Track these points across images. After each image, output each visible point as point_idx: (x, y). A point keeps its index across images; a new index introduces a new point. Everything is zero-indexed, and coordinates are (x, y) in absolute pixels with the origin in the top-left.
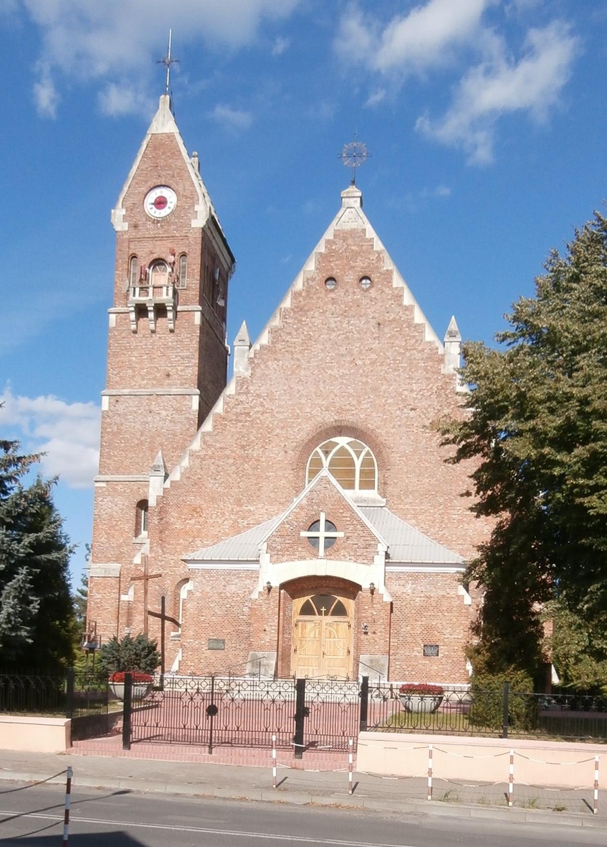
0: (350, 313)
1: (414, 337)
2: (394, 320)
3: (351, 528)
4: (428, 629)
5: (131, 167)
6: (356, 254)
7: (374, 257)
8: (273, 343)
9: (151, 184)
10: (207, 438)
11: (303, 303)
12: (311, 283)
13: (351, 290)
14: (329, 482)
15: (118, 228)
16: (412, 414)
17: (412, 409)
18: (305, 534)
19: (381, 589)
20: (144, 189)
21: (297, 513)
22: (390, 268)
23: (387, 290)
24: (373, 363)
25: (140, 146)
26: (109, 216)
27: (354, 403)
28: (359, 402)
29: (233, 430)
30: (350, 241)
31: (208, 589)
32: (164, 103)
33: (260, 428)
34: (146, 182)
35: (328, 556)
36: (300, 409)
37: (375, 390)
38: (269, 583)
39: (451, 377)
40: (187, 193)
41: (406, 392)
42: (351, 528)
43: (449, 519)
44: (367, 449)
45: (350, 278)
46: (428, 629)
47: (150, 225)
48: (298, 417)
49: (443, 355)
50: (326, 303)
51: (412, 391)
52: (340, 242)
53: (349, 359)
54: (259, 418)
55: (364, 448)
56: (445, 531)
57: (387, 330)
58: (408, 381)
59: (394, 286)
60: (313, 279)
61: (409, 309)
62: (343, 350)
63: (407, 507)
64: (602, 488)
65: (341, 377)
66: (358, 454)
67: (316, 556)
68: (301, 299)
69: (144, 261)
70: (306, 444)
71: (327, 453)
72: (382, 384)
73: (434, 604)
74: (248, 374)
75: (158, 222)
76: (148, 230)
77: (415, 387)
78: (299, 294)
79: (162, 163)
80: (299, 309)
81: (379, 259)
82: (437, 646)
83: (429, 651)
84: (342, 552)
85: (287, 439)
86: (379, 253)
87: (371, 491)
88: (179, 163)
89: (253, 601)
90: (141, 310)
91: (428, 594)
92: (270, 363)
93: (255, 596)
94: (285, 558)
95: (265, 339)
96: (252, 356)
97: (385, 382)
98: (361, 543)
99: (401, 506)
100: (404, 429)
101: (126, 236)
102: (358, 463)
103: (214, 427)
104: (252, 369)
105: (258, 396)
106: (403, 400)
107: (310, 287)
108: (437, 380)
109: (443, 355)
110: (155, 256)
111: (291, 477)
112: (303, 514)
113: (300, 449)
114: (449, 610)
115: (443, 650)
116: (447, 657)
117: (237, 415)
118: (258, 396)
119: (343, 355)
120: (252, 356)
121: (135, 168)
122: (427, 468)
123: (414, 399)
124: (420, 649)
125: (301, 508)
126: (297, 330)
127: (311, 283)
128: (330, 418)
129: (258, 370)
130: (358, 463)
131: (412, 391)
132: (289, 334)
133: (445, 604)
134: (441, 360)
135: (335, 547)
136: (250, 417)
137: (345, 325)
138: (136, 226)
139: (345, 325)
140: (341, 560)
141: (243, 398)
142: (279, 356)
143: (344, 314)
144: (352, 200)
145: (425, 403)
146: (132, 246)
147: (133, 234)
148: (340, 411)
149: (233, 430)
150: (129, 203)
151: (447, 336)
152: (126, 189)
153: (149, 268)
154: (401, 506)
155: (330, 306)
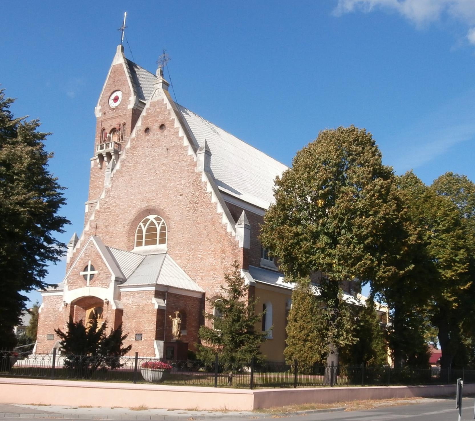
0: (156, 145)
1: (183, 154)
2: (174, 146)
3: (101, 268)
4: (139, 324)
5: (104, 84)
6: (159, 113)
7: (166, 113)
8: (121, 167)
9: (112, 91)
10: (92, 224)
11: (135, 144)
12: (139, 133)
13: (156, 133)
14: (93, 244)
15: (97, 116)
16: (181, 197)
17: (181, 195)
18: (83, 273)
19: (112, 302)
20: (109, 94)
21: (80, 262)
22: (174, 118)
23: (172, 130)
24: (164, 172)
25: (108, 72)
26: (94, 110)
27: (155, 195)
28: (157, 194)
30: (157, 107)
31: (49, 307)
34: (110, 90)
36: (131, 202)
37: (164, 186)
38: (38, 303)
39: (200, 174)
40: (127, 92)
41: (178, 186)
42: (101, 268)
43: (196, 258)
44: (163, 220)
45: (156, 126)
46: (139, 324)
48: (130, 207)
49: (196, 162)
50: (145, 142)
51: (181, 184)
52: (152, 108)
53: (153, 171)
54: (113, 210)
55: (161, 220)
56: (194, 265)
58: (180, 179)
60: (140, 130)
61: (181, 138)
63: (177, 252)
64: (346, 227)
65: (150, 181)
66: (159, 223)
67: (86, 285)
68: (134, 142)
69: (108, 131)
70: (133, 221)
71: (145, 225)
72: (168, 183)
73: (141, 309)
74: (110, 186)
75: (114, 109)
76: (109, 114)
77: (183, 182)
78: (133, 139)
79: (117, 79)
80: (133, 148)
81: (169, 114)
82: (141, 334)
83: (138, 337)
84: (97, 282)
85: (125, 219)
86: (169, 110)
87: (155, 246)
88: (124, 77)
90: (101, 157)
92: (119, 179)
93: (61, 309)
94: (74, 287)
95: (118, 167)
97: (169, 181)
100: (177, 207)
101: (100, 120)
102: (159, 229)
103: (95, 217)
105: (114, 197)
107: (138, 135)
108: (193, 176)
109: (196, 162)
110: (112, 127)
111: (126, 241)
112: (82, 262)
113: (130, 224)
115: (144, 336)
116: (146, 340)
117: (105, 209)
118: (114, 197)
119: (151, 169)
120: (112, 176)
121: (105, 84)
122: (187, 228)
124: (134, 336)
125: (82, 259)
126: (131, 159)
127: (139, 133)
128: (143, 205)
129: (114, 184)
130: (159, 229)
131: (181, 184)
132: (128, 162)
133: (146, 308)
134: (195, 165)
135: (94, 279)
137: (152, 153)
138: (105, 114)
139: (152, 153)
140: (96, 286)
141: (107, 200)
143: (152, 147)
144: (158, 85)
145: (187, 191)
146: (103, 124)
147: (104, 117)
149: (103, 218)
150: (102, 103)
151: (198, 150)
152: (101, 95)
153: (110, 133)
155: (146, 143)
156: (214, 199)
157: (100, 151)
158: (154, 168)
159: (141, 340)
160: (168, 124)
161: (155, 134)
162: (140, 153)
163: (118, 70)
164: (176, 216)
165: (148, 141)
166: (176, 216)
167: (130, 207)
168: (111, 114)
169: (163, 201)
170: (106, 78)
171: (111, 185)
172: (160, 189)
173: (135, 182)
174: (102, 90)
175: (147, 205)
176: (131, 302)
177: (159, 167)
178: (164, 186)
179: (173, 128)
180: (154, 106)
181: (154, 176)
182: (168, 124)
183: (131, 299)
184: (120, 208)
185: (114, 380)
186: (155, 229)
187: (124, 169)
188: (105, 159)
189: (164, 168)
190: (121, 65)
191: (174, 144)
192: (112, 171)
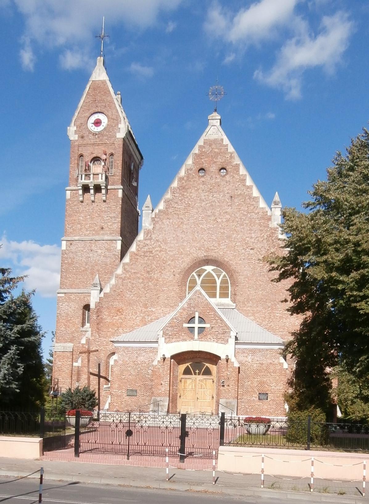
0: (214, 190)
1: (253, 205)
2: (241, 194)
4: (261, 383)
6: (218, 154)
7: (228, 156)
9: (92, 111)
11: (185, 184)
12: (190, 172)
13: (214, 176)
14: (201, 293)
15: (72, 138)
16: (252, 252)
18: (186, 325)
19: (232, 359)
20: (87, 114)
22: (238, 163)
23: (236, 176)
24: (228, 221)
25: (85, 88)
26: (66, 131)
27: (216, 245)
28: (219, 245)
29: (142, 262)
30: (213, 146)
32: (100, 61)
33: (158, 261)
34: (89, 110)
35: (200, 339)
36: (183, 249)
39: (275, 229)
40: (114, 117)
42: (214, 321)
43: (274, 316)
44: (224, 273)
45: (214, 169)
46: (261, 383)
47: (91, 136)
48: (182, 253)
49: (271, 216)
50: (199, 184)
51: (251, 238)
52: (207, 147)
53: (213, 218)
54: (158, 254)
55: (222, 273)
57: (236, 200)
58: (249, 232)
59: (241, 173)
60: (191, 169)
61: (250, 188)
62: (209, 213)
66: (219, 276)
67: (193, 339)
68: (184, 181)
70: (187, 270)
71: (199, 276)
72: (233, 234)
74: (151, 227)
75: (96, 134)
76: (90, 139)
77: (253, 235)
78: (182, 178)
79: (98, 98)
80: (182, 188)
81: (231, 157)
82: (267, 394)
83: (262, 397)
84: (209, 336)
86: (231, 153)
88: (109, 99)
89: (154, 367)
90: (86, 189)
91: (261, 362)
92: (164, 221)
93: (155, 363)
94: (174, 340)
95: (161, 206)
96: (154, 216)
98: (221, 331)
99: (245, 308)
100: (246, 261)
101: (76, 143)
102: (218, 282)
103: (131, 260)
104: (154, 224)
106: (246, 244)
107: (189, 174)
108: (267, 231)
109: (271, 216)
110: (94, 155)
111: (177, 291)
112: (185, 313)
113: (183, 273)
114: (274, 372)
115: (270, 396)
116: (273, 400)
117: (144, 252)
119: (209, 216)
120: (154, 216)
121: (82, 101)
122: (260, 285)
123: (253, 243)
124: (256, 395)
127: (190, 172)
128: (202, 254)
129: (157, 225)
130: (218, 282)
131: (251, 238)
132: (177, 203)
133: (272, 368)
134: (269, 219)
136: (152, 253)
137: (210, 198)
138: (82, 137)
139: (210, 198)
140: (208, 341)
141: (148, 242)
142: (170, 216)
143: (210, 191)
145: (259, 245)
147: (81, 142)
148: (208, 250)
149: (142, 262)
150: (78, 123)
152: (76, 114)
153: (91, 162)
154: (245, 308)
156: (133, 248)
157: (84, 181)
158: (214, 214)
159: (267, 399)
160: (231, 168)
161: (213, 177)
162: (194, 195)
163: (99, 87)
164: (246, 270)
165: (204, 183)
166: (246, 270)
167: (182, 253)
168: (91, 139)
169: (228, 252)
170: (82, 95)
171: (152, 226)
172: (223, 240)
173: (188, 227)
174: (76, 107)
175: (205, 254)
176: (250, 360)
177: (220, 214)
178: (229, 237)
179: (238, 174)
180: (210, 145)
181: (214, 224)
182: (231, 168)
183: (249, 357)
184: (166, 253)
185: (24, 434)
186: (215, 282)
187: (170, 210)
188: (92, 191)
189: (228, 217)
190: (104, 82)
191: (239, 192)
192: (153, 211)
